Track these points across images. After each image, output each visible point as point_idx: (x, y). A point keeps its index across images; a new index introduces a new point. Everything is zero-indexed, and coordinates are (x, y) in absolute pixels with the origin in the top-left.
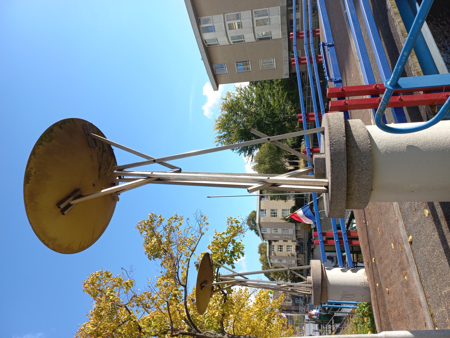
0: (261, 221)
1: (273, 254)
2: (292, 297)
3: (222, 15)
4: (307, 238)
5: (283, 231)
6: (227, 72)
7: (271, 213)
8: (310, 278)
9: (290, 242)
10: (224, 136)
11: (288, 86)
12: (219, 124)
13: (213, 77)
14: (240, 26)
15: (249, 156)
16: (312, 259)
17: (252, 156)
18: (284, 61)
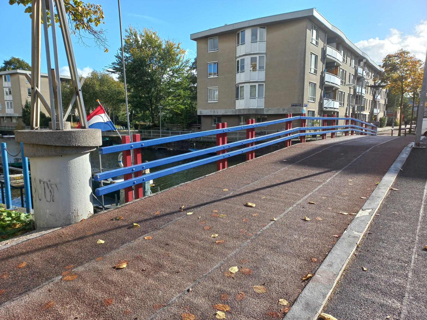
0: (21, 77)
3: (265, 52)
4: (3, 130)
5: (9, 102)
6: (208, 52)
11: (190, 114)
12: (151, 36)
13: (201, 36)
18: (214, 111)
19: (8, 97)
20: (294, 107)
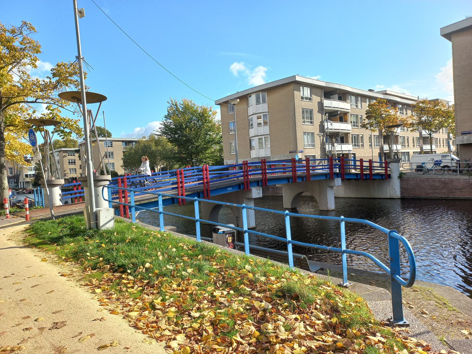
1: (64, 154)
2: (17, 176)
8: (54, 179)
9: (79, 171)
10: (177, 109)
17: (160, 135)
20: (291, 154)
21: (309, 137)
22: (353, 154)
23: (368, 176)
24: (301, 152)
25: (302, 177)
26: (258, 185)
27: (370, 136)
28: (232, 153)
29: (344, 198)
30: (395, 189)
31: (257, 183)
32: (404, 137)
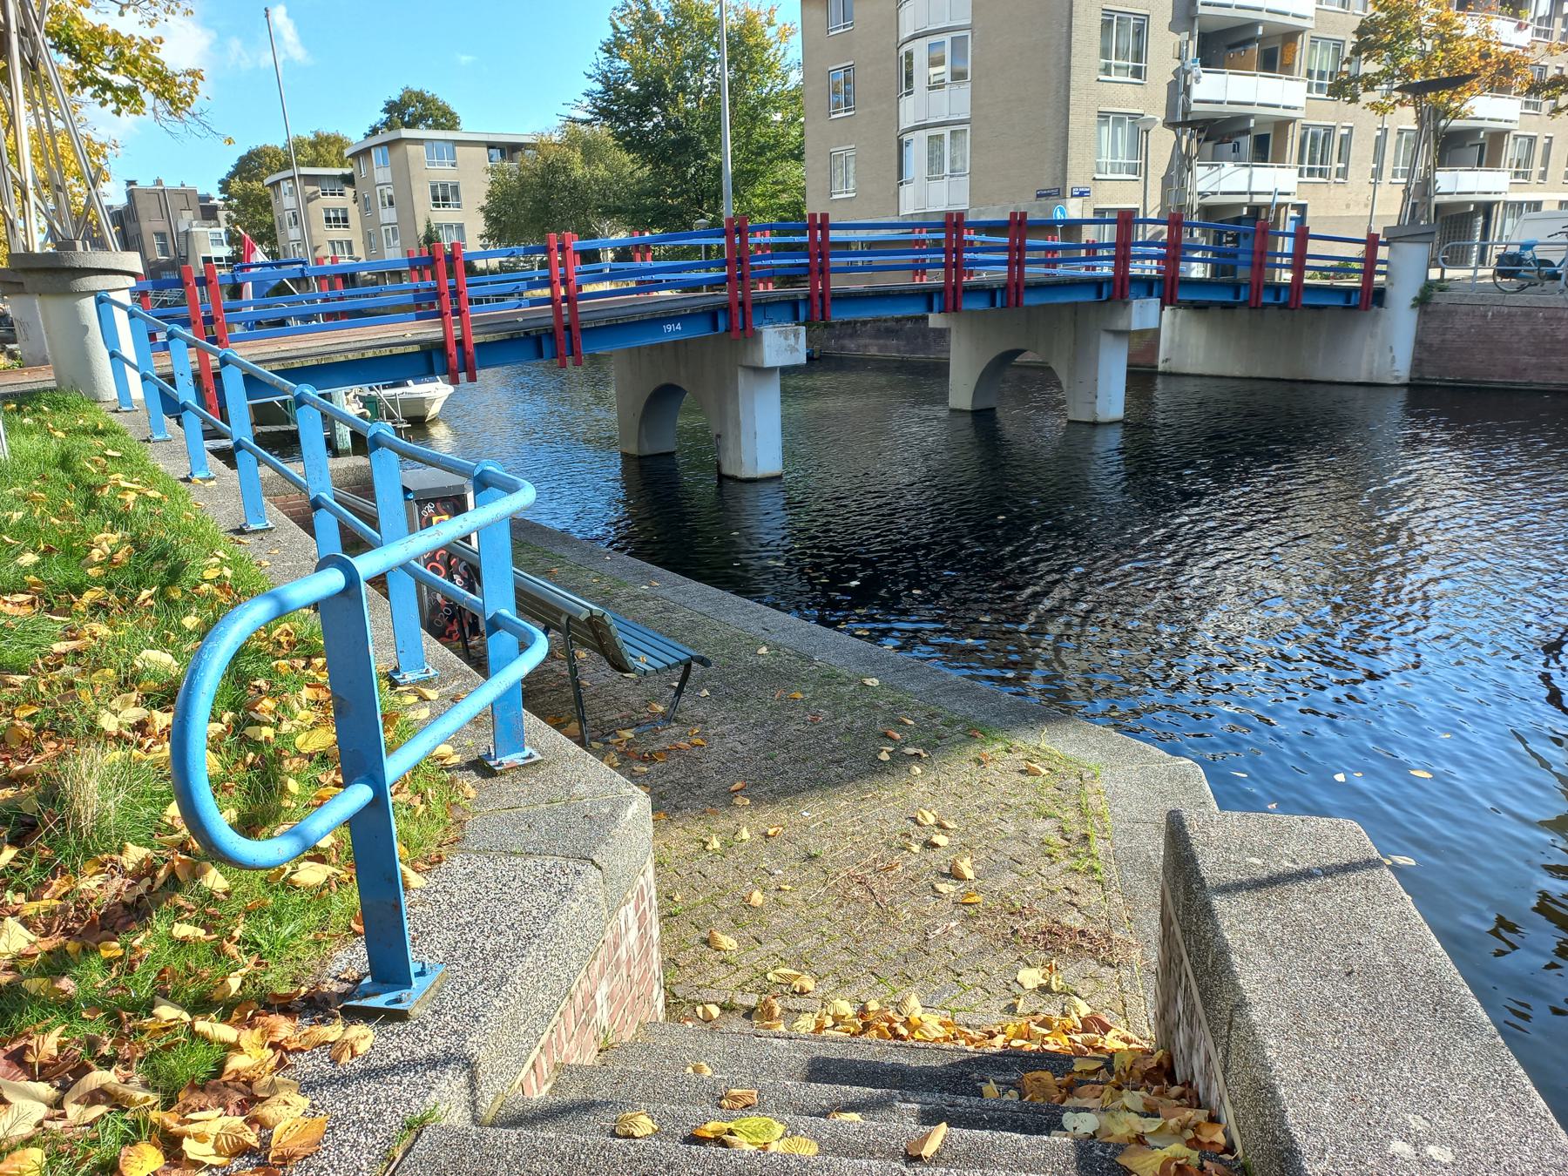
0: (411, 148)
1: (310, 189)
5: (390, 227)
7: (444, 186)
14: (934, 87)
15: (590, 108)
16: (483, 367)
19: (386, 211)
21: (1123, 134)
22: (1294, 206)
23: (1283, 294)
24: (1081, 194)
25: (988, 292)
26: (795, 318)
27: (1379, 133)
28: (835, 197)
29: (1201, 376)
30: (1391, 349)
31: (791, 309)
32: (1532, 140)
